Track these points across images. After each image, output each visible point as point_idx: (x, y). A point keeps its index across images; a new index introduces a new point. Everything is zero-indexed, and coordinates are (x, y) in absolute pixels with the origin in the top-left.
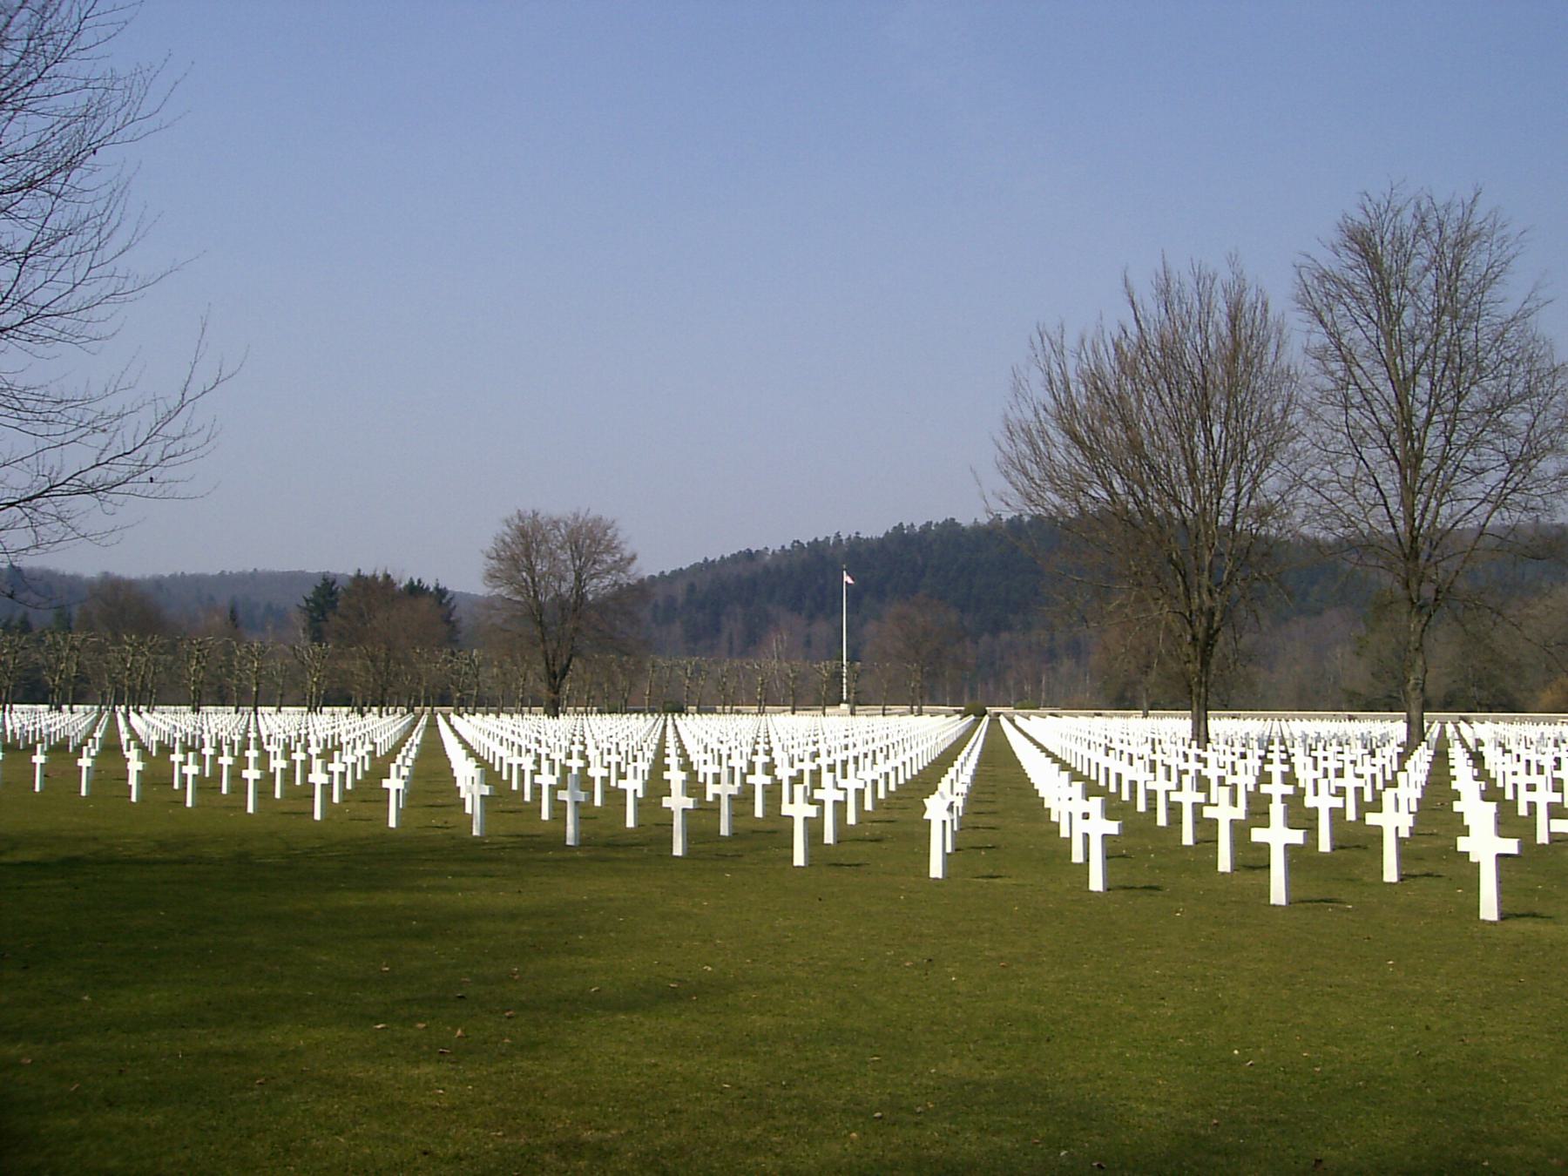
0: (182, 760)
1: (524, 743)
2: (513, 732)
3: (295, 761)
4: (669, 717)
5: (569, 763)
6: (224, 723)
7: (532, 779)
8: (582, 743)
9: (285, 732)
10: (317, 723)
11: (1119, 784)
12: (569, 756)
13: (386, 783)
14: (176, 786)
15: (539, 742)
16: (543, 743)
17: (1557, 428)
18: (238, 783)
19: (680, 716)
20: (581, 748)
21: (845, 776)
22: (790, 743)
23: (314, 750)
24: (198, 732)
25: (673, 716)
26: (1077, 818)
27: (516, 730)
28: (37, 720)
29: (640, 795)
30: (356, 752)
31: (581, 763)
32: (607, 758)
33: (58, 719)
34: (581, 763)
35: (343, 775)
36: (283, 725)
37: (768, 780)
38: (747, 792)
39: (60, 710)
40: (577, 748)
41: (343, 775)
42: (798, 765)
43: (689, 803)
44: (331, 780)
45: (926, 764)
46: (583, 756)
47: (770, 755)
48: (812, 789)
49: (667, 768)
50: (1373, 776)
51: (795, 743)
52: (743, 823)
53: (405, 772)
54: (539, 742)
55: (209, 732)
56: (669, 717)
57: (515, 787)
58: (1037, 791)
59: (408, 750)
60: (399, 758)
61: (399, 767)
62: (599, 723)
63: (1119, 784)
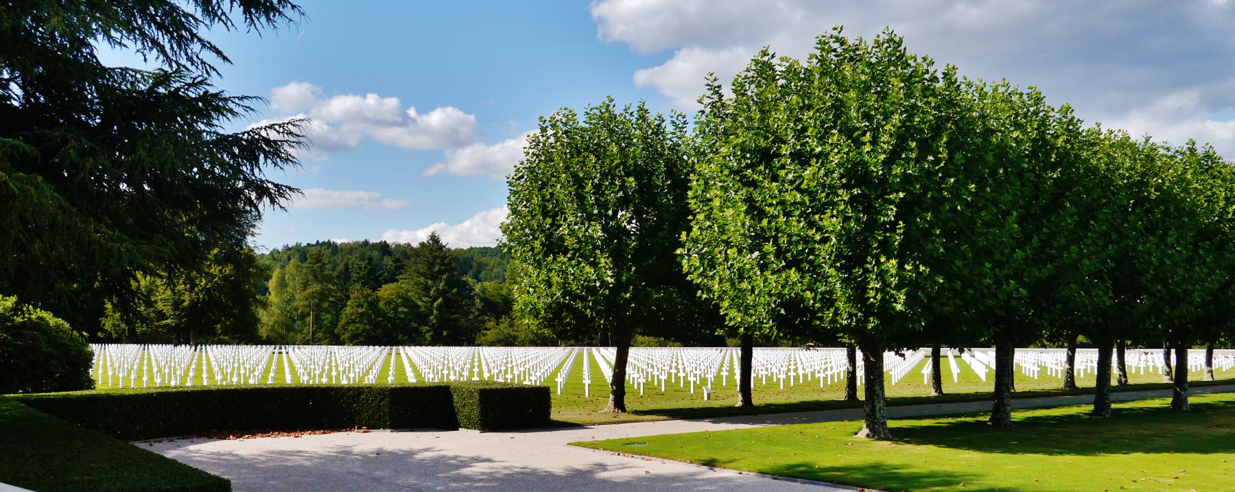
1: (643, 359)
4: (146, 346)
5: (671, 371)
7: (777, 376)
8: (676, 362)
11: (1034, 374)
12: (671, 368)
13: (556, 380)
15: (652, 360)
16: (654, 361)
17: (52, 174)
18: (677, 378)
20: (676, 365)
23: (514, 364)
24: (442, 360)
26: (760, 370)
27: (651, 357)
28: (509, 355)
29: (713, 380)
31: (676, 371)
32: (692, 365)
33: (354, 350)
34: (676, 371)
35: (363, 369)
37: (795, 374)
38: (788, 377)
39: (810, 350)
40: (674, 365)
41: (363, 369)
42: (813, 368)
43: (645, 381)
45: (1227, 368)
46: (676, 368)
48: (505, 375)
49: (722, 371)
50: (704, 370)
51: (813, 360)
53: (563, 375)
54: (652, 360)
60: (564, 367)
63: (1034, 374)
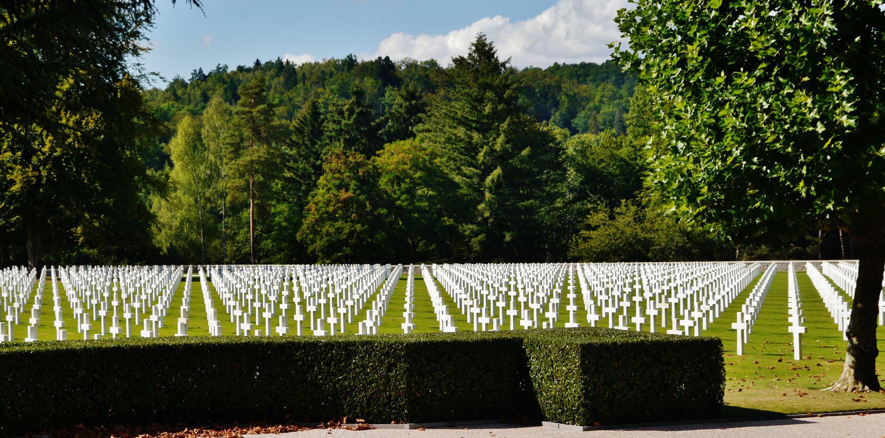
0: (497, 303)
2: (483, 274)
3: (635, 302)
4: (53, 269)
6: (535, 273)
9: (612, 282)
10: (649, 271)
13: (734, 326)
14: (232, 321)
19: (86, 269)
21: (660, 301)
22: (606, 280)
25: (56, 268)
30: (678, 296)
35: (353, 307)
36: (610, 275)
44: (347, 311)
46: (516, 289)
47: (632, 287)
52: (338, 334)
53: (748, 317)
55: (522, 282)
56: (53, 269)
57: (463, 313)
58: (830, 313)
59: (757, 291)
61: (747, 307)
62: (496, 267)
